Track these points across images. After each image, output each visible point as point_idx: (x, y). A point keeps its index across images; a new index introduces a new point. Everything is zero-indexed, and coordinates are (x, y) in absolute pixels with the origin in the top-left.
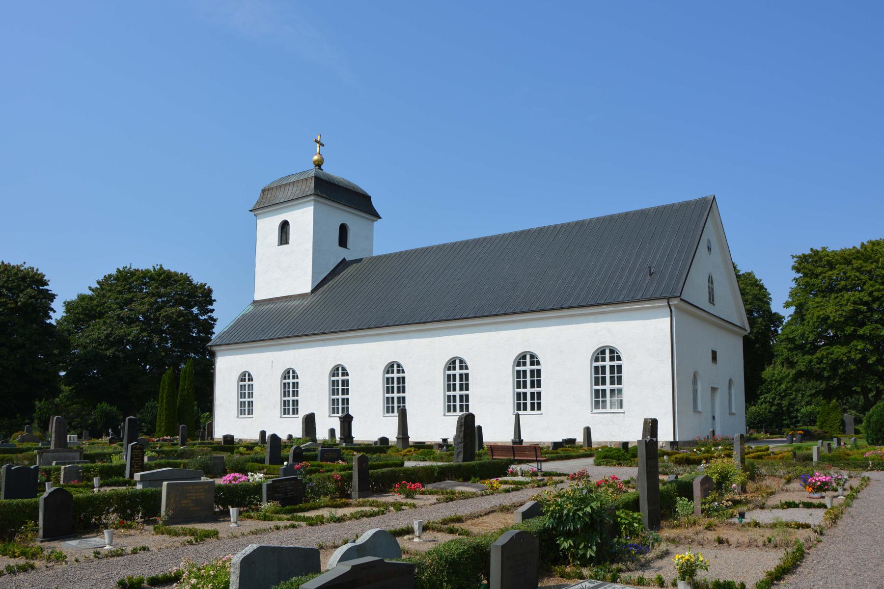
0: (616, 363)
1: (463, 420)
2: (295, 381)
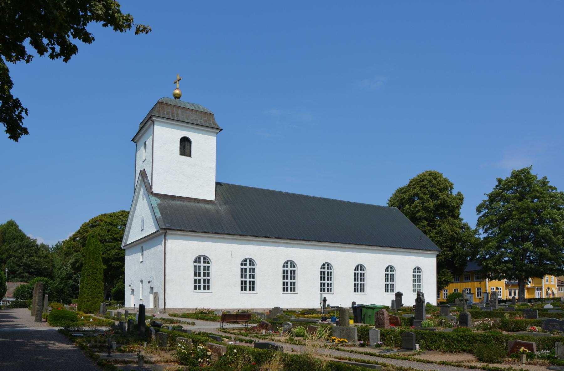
0: (252, 267)
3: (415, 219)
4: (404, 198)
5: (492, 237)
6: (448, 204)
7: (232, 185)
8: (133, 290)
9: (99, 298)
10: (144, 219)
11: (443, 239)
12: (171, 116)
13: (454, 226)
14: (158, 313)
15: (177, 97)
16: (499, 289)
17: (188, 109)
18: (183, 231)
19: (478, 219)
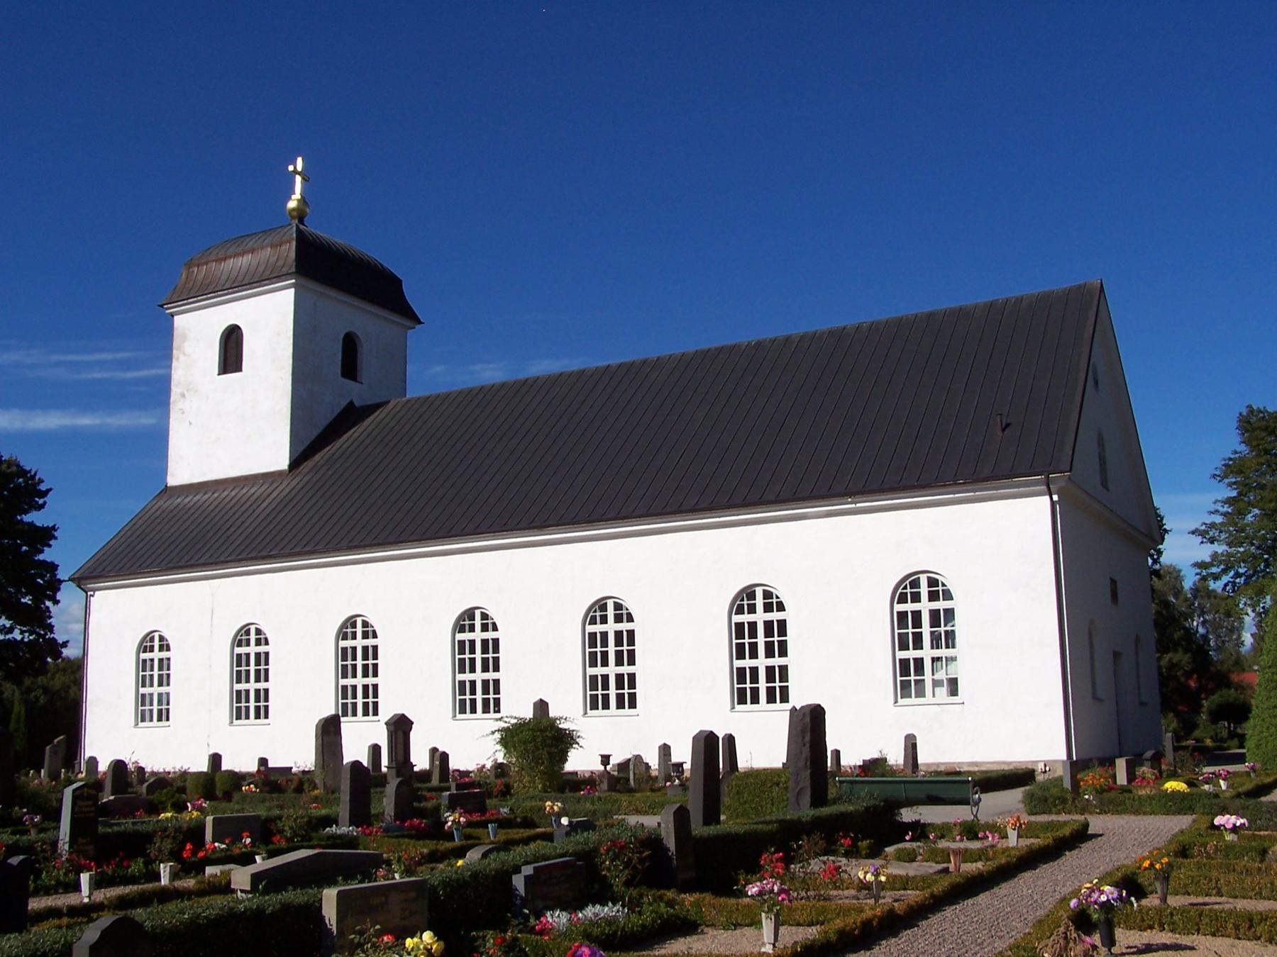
1: (808, 719)
2: (262, 649)
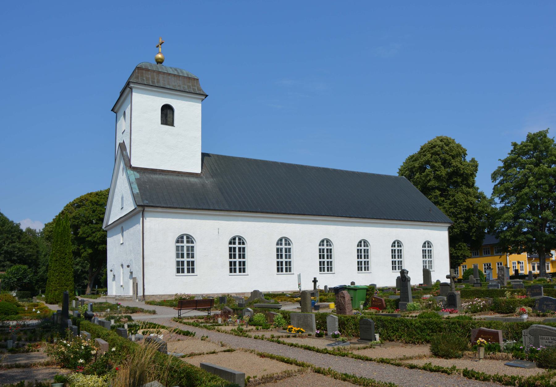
0: (242, 246)
3: (426, 190)
4: (414, 167)
5: (509, 206)
6: (462, 172)
7: (221, 156)
8: (114, 276)
9: (68, 286)
10: (124, 196)
11: (458, 210)
12: (151, 82)
13: (468, 195)
14: (137, 300)
15: (160, 62)
16: (521, 263)
17: (170, 74)
18: (163, 207)
19: (494, 187)
